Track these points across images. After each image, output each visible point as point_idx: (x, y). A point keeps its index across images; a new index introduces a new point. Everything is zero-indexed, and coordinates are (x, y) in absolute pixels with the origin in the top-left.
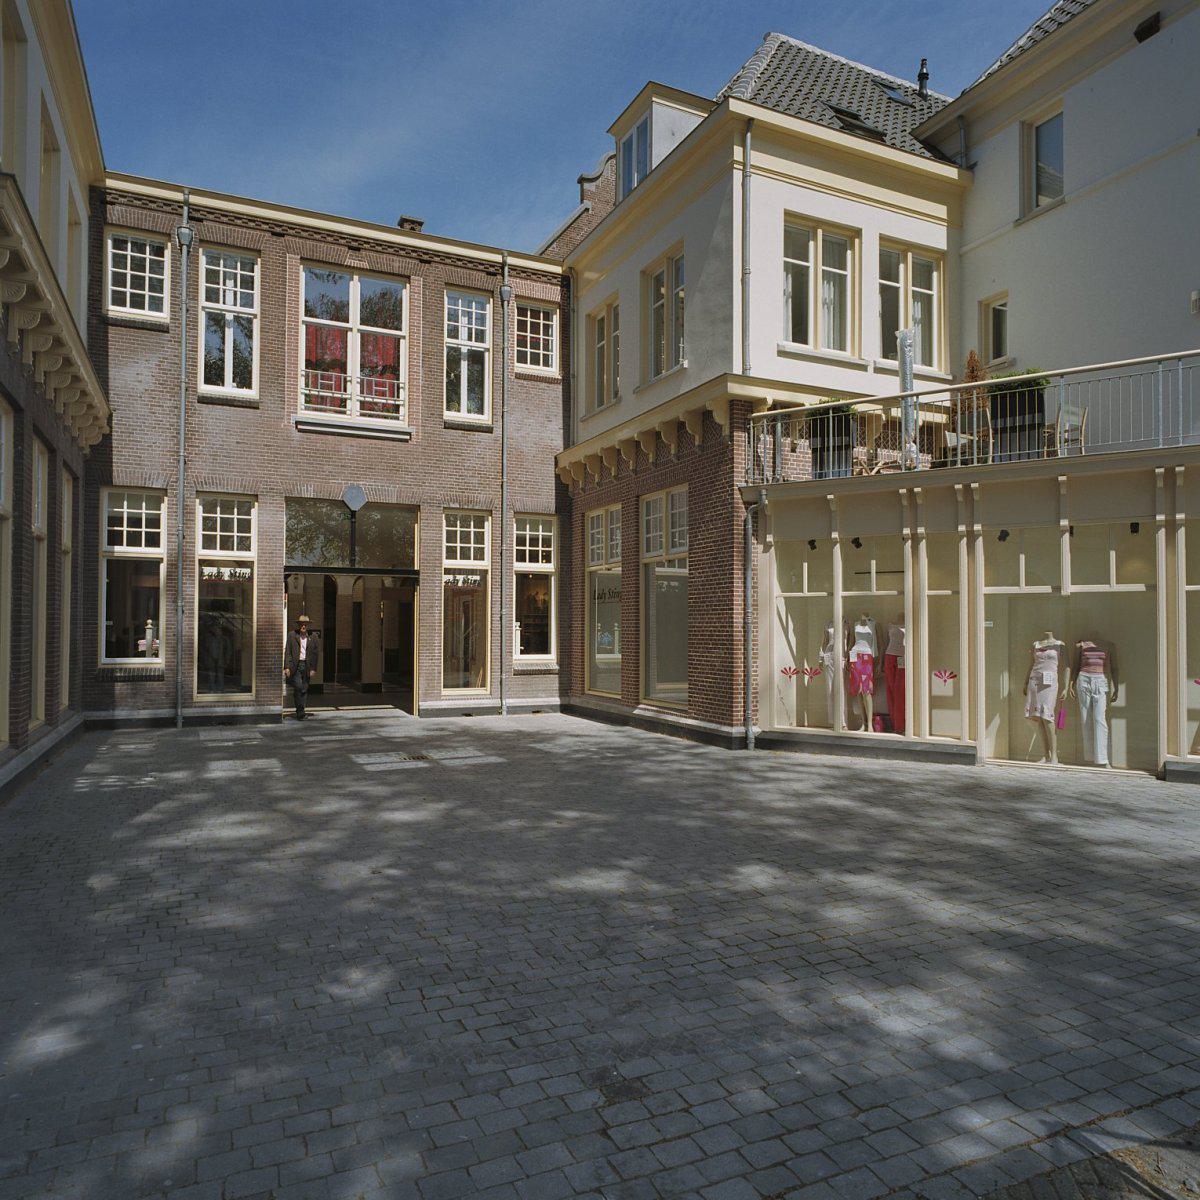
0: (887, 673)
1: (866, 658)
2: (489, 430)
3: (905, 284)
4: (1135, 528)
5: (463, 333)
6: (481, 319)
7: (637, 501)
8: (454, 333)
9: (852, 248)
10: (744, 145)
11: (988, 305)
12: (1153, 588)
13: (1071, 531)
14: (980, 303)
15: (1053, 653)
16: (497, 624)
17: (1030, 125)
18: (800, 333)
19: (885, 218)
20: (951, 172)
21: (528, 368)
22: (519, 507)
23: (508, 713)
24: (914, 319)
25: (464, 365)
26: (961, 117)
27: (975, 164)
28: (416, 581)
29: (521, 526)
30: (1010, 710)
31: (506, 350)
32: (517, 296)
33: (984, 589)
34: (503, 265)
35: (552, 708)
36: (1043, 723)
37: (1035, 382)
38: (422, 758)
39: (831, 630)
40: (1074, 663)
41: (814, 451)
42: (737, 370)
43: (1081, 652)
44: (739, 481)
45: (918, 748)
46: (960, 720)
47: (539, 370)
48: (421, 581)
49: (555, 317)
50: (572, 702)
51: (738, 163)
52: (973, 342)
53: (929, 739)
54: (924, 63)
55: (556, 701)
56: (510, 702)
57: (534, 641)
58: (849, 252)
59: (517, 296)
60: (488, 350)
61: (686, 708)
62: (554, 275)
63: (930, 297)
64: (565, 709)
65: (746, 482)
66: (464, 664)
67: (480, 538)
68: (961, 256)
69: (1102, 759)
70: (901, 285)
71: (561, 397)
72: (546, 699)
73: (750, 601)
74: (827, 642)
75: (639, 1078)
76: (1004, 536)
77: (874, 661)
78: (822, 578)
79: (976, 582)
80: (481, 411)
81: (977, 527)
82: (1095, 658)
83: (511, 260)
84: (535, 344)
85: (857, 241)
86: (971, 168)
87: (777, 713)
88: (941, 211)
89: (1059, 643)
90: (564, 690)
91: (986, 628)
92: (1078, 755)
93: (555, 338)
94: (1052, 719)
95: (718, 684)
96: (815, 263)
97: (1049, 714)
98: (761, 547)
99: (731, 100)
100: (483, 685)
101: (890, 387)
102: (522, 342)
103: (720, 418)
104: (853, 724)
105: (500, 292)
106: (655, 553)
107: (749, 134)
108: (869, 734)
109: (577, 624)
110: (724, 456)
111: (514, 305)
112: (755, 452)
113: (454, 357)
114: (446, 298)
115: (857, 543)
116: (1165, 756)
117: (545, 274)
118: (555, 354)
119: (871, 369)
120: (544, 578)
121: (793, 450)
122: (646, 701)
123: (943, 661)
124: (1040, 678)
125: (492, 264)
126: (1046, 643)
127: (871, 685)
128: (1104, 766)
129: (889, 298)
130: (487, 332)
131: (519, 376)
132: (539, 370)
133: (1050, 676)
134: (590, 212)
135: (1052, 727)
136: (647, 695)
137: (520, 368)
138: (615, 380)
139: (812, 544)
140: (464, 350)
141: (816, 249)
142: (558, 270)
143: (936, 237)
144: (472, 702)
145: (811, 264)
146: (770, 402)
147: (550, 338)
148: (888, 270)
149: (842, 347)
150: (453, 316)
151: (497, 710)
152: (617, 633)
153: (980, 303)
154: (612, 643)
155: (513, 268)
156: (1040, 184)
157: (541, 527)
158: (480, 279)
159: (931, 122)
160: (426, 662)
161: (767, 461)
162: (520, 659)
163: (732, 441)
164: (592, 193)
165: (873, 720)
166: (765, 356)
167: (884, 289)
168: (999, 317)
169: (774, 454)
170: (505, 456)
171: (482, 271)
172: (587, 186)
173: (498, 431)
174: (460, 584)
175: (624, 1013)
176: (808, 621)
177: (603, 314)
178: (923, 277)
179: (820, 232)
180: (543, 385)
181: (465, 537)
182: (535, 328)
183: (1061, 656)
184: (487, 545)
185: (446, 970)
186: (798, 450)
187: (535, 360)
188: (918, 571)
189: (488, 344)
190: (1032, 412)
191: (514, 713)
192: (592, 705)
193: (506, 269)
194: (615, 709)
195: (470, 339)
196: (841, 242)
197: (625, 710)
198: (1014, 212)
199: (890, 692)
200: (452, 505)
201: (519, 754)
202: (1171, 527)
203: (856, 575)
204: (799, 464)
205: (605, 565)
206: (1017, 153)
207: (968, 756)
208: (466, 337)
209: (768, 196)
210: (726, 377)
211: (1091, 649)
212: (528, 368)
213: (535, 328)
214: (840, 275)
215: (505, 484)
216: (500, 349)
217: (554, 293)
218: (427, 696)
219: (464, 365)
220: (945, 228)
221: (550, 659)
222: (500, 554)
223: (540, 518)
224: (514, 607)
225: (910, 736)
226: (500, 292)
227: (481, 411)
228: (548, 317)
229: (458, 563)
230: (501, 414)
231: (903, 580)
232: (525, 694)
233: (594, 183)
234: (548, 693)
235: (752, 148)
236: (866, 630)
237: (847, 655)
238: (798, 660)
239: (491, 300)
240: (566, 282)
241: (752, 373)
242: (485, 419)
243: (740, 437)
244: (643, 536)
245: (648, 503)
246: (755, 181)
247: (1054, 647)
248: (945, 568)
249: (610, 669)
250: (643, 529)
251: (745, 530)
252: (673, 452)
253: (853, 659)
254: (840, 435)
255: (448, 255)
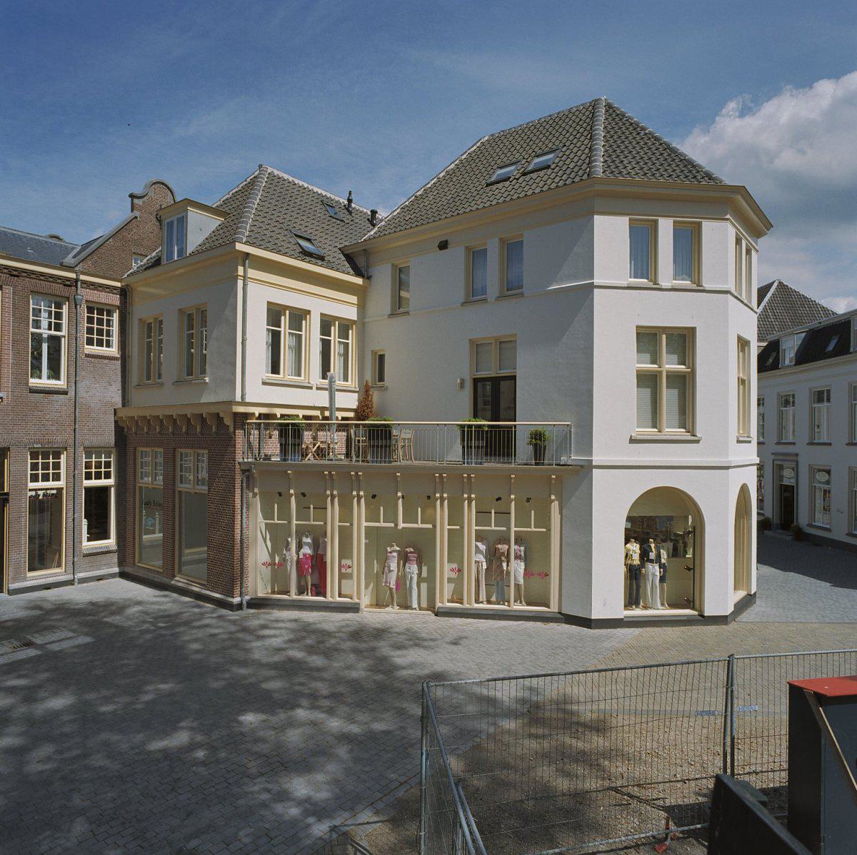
0: (318, 563)
1: (307, 556)
2: (65, 393)
3: (334, 337)
4: (429, 497)
5: (45, 324)
6: (59, 316)
7: (174, 451)
8: (37, 324)
9: (306, 320)
10: (244, 265)
11: (376, 353)
12: (434, 526)
13: (403, 497)
14: (372, 351)
15: (395, 554)
16: (71, 514)
17: (376, 353)
18: (275, 369)
19: (322, 303)
20: (359, 281)
21: (95, 349)
22: (87, 444)
23: (79, 583)
24: (339, 354)
25: (45, 346)
26: (364, 250)
27: (371, 277)
28: (6, 500)
29: (89, 455)
30: (375, 579)
31: (78, 339)
32: (86, 301)
33: (365, 524)
34: (77, 280)
35: (112, 576)
36: (391, 589)
37: (388, 426)
38: (29, 644)
39: (289, 539)
40: (404, 558)
41: (281, 445)
42: (238, 398)
43: (407, 553)
44: (239, 459)
45: (332, 605)
46: (353, 587)
47: (103, 350)
48: (11, 500)
49: (115, 314)
50: (126, 570)
51: (240, 276)
52: (368, 376)
53: (339, 599)
54: (350, 193)
55: (116, 570)
56: (81, 575)
57: (99, 530)
58: (304, 322)
59: (86, 301)
60: (64, 337)
61: (206, 583)
62: (115, 288)
63: (348, 343)
64: (123, 575)
65: (243, 458)
66: (43, 554)
67: (57, 466)
68: (364, 323)
69: (415, 605)
70: (332, 338)
71: (120, 370)
72: (107, 570)
73: (244, 525)
74: (287, 545)
75: (194, 849)
76: (374, 496)
77: (312, 557)
78: (285, 514)
79: (360, 511)
80: (57, 377)
81: (362, 493)
82: (413, 557)
83: (82, 277)
84: (100, 332)
85: (308, 316)
86: (369, 278)
87: (257, 583)
88: (354, 299)
89: (398, 549)
90: (120, 564)
91: (366, 544)
92: (406, 606)
93: (115, 329)
94: (394, 587)
95: (226, 569)
96: (284, 328)
97: (393, 585)
98: (251, 494)
99: (237, 243)
100: (59, 565)
101: (322, 399)
102: (90, 331)
103: (228, 421)
104: (301, 591)
105: (75, 299)
106: (185, 486)
107: (247, 261)
108: (309, 598)
109: (130, 519)
110: (229, 442)
111: (84, 307)
112: (248, 440)
113: (37, 339)
114: (31, 301)
115: (304, 495)
116: (438, 605)
117: (108, 287)
118: (115, 339)
119: (314, 388)
120: (105, 490)
121: (270, 437)
122: (179, 575)
123: (345, 551)
124: (389, 567)
125: (68, 279)
126: (392, 549)
127: (310, 570)
128: (415, 609)
129: (326, 346)
130: (64, 325)
131: (88, 356)
132: (103, 350)
133: (394, 566)
134: (139, 219)
135: (394, 590)
136: (180, 571)
137: (90, 349)
138: (159, 357)
139: (280, 494)
140: (45, 336)
141: (285, 320)
142: (118, 284)
143: (351, 313)
144: (51, 579)
145: (282, 329)
146: (257, 415)
147: (111, 328)
148: (325, 329)
149: (299, 375)
150: (37, 312)
151: (71, 583)
152: (157, 519)
153: (372, 351)
154: (153, 525)
155: (84, 282)
156: (398, 307)
157: (103, 455)
158: (58, 289)
159: (352, 247)
160: (14, 556)
161: (256, 444)
162: (87, 545)
163: (235, 435)
164: (140, 206)
165: (311, 589)
166: (256, 388)
167: (322, 340)
168: (382, 357)
169: (259, 441)
170: (77, 411)
171: (60, 283)
172: (136, 201)
173: (72, 393)
174: (41, 497)
175: (185, 819)
176: (278, 538)
177: (152, 321)
178: (344, 333)
179: (287, 312)
180: (106, 361)
181: (46, 467)
182: (100, 322)
183: (399, 555)
184: (63, 471)
185: (101, 817)
186: (273, 437)
187: (100, 343)
188: (334, 511)
189: (64, 332)
190: (386, 439)
191: (83, 583)
192: (141, 574)
193: (79, 283)
194: (158, 579)
195: (50, 329)
196: (299, 317)
197: (165, 580)
198: (388, 310)
199: (320, 574)
200: (35, 446)
201: (91, 617)
202: (442, 499)
203: (303, 511)
204: (272, 447)
205: (150, 478)
206: (390, 283)
207: (355, 608)
208: (47, 327)
209: (258, 294)
210: (232, 403)
211: (411, 552)
212: (95, 349)
213: (100, 322)
214: (299, 334)
215: (77, 430)
216: (74, 338)
217: (115, 300)
218: (15, 580)
219: (45, 346)
220: (356, 309)
221: (111, 542)
222: (73, 478)
223: (103, 450)
224: (83, 513)
225: (329, 599)
226: (75, 299)
227: (57, 377)
228: (110, 313)
229: (41, 484)
230: (74, 379)
231: (326, 513)
232: (92, 568)
233: (142, 200)
234: (109, 565)
235: (249, 267)
236: (309, 540)
237: (298, 554)
238: (272, 556)
239: (67, 303)
240: (124, 293)
241: (247, 400)
242: (61, 384)
243: (239, 433)
244: (178, 473)
245: (181, 453)
246: (250, 285)
247: (394, 551)
248: (346, 514)
249: (153, 545)
250: (178, 469)
251: (242, 486)
252: (198, 430)
253: (301, 556)
254: (295, 438)
255: (33, 272)
